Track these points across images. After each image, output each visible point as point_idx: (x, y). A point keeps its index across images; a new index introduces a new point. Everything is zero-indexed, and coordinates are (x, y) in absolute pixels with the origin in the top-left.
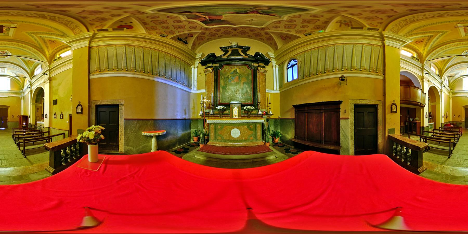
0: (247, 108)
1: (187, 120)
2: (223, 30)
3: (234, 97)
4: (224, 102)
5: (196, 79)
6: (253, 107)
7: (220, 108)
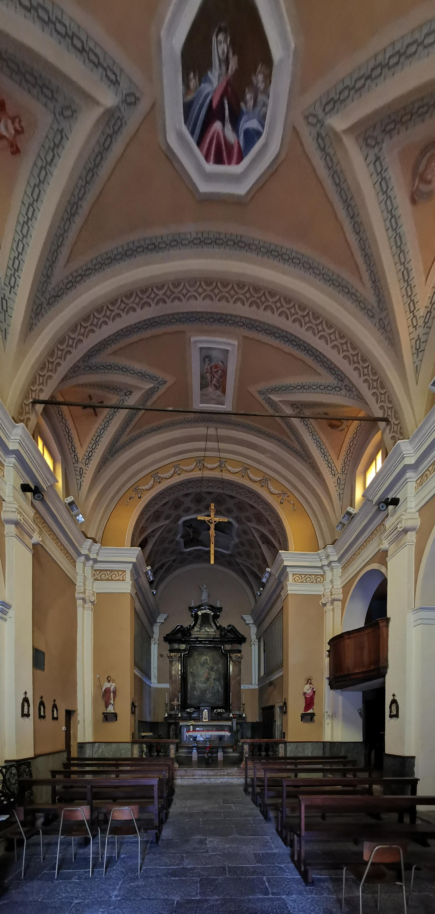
5: (156, 665)
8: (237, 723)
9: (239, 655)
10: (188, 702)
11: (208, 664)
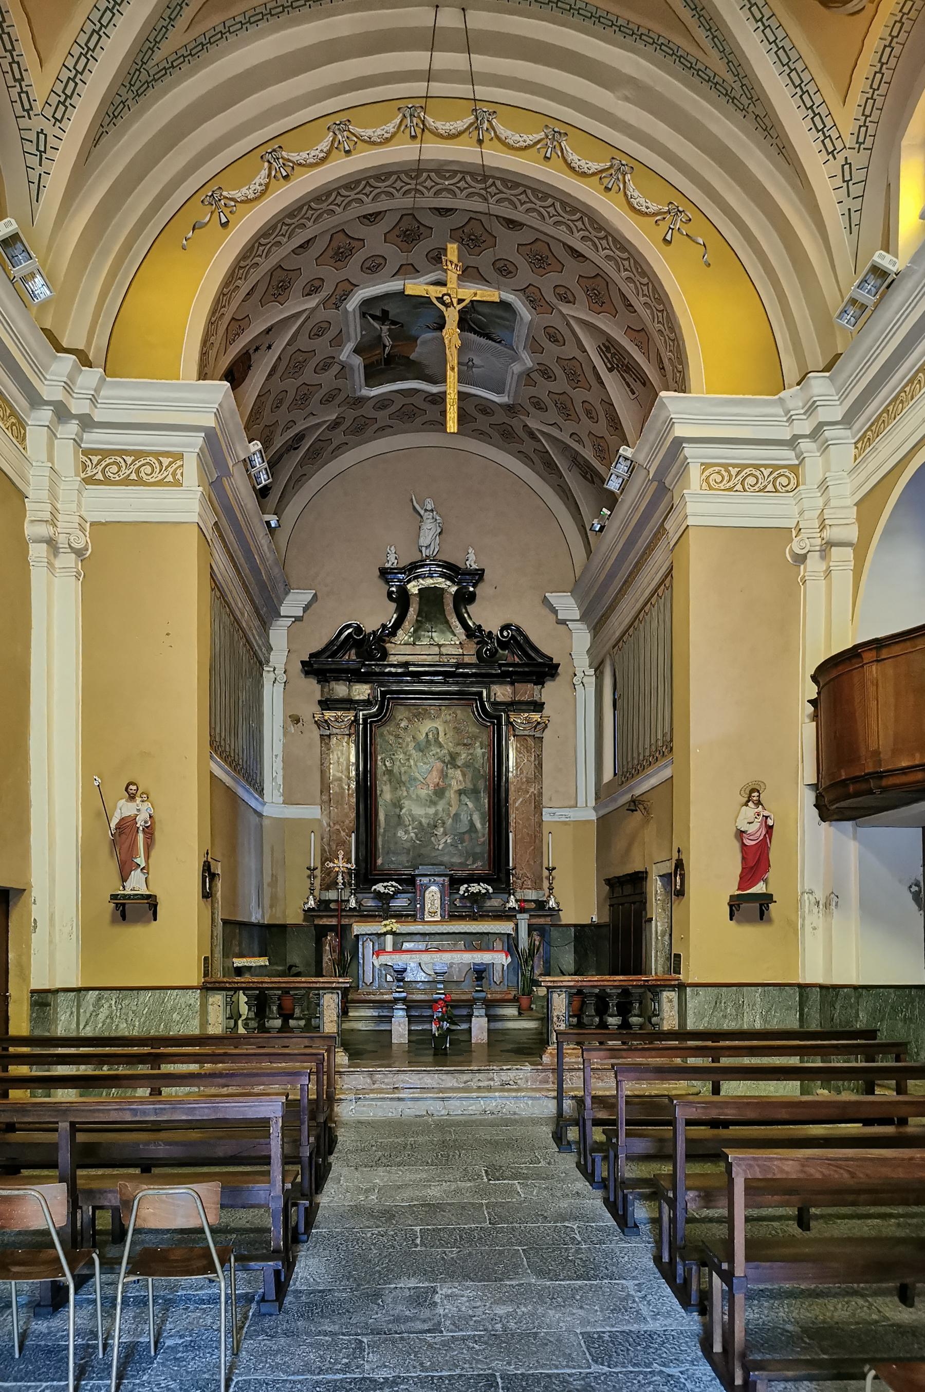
0: (468, 891)
2: (400, 401)
3: (429, 848)
5: (278, 749)
6: (489, 888)
8: (531, 929)
9: (536, 717)
10: (379, 861)
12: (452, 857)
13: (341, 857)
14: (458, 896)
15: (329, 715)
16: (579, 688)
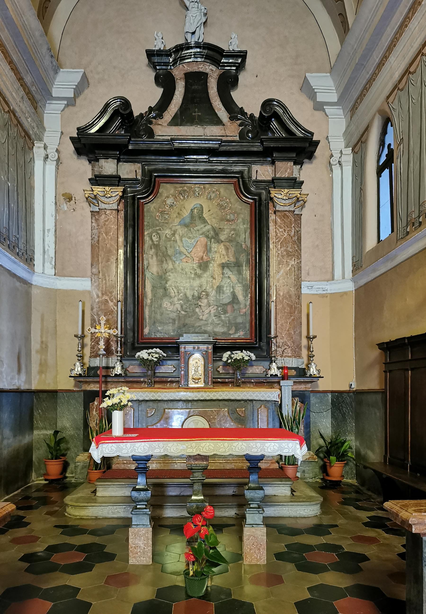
0: (231, 358)
1: (24, 394)
4: (158, 335)
5: (50, 224)
6: (252, 355)
7: (150, 358)
8: (295, 394)
9: (295, 192)
10: (146, 331)
11: (204, 221)
12: (174, 105)
13: (103, 322)
14: (221, 363)
15: (98, 190)
16: (337, 170)
